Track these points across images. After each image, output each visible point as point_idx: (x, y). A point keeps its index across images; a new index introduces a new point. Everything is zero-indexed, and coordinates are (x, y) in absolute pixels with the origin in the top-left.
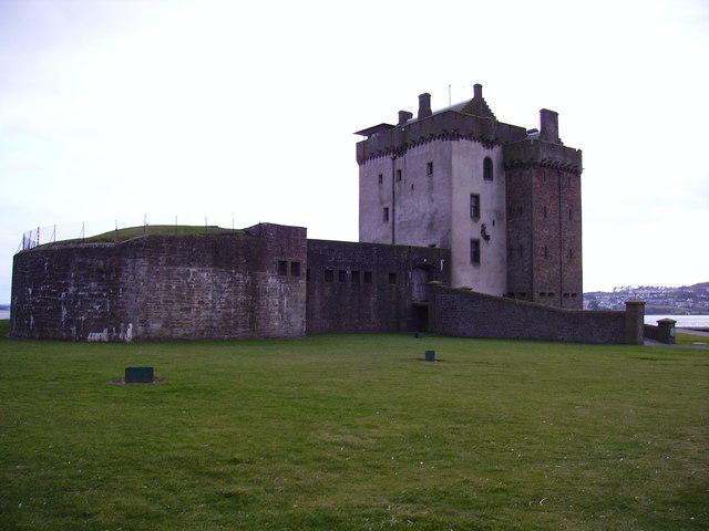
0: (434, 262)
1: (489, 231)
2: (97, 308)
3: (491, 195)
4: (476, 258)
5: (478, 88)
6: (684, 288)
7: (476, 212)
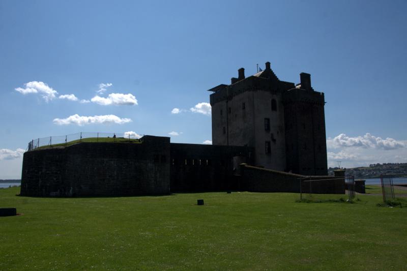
0: (248, 153)
1: (275, 137)
2: (55, 179)
3: (276, 119)
4: (269, 152)
5: (268, 64)
6: (378, 165)
7: (268, 129)
